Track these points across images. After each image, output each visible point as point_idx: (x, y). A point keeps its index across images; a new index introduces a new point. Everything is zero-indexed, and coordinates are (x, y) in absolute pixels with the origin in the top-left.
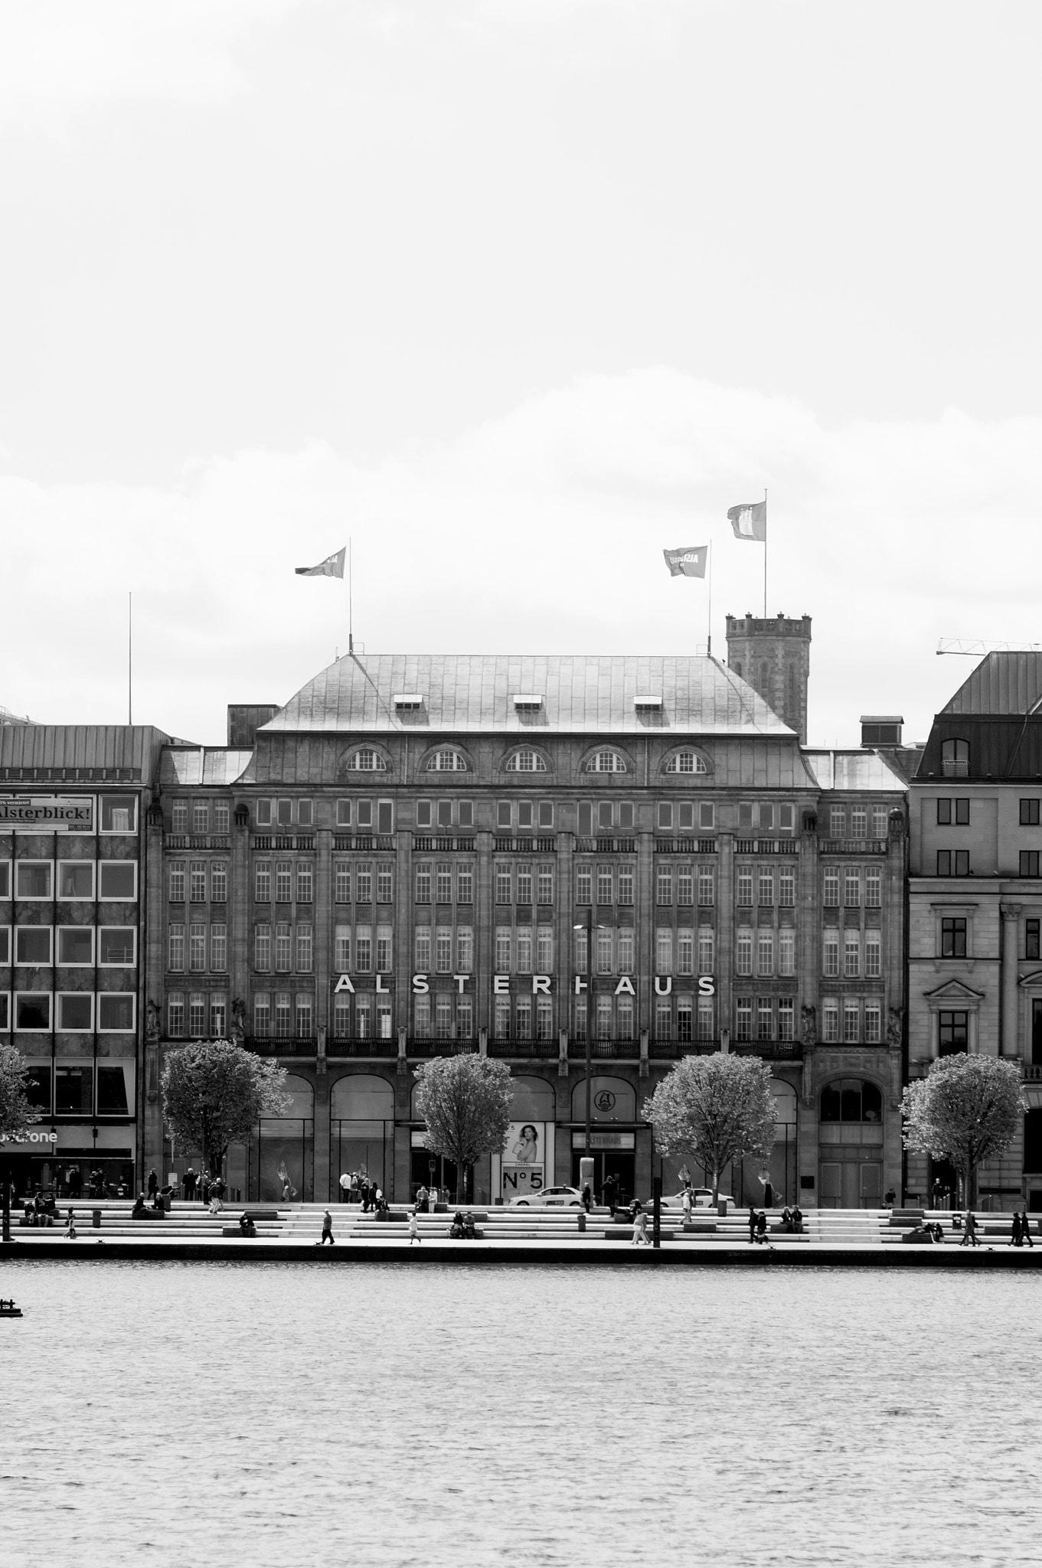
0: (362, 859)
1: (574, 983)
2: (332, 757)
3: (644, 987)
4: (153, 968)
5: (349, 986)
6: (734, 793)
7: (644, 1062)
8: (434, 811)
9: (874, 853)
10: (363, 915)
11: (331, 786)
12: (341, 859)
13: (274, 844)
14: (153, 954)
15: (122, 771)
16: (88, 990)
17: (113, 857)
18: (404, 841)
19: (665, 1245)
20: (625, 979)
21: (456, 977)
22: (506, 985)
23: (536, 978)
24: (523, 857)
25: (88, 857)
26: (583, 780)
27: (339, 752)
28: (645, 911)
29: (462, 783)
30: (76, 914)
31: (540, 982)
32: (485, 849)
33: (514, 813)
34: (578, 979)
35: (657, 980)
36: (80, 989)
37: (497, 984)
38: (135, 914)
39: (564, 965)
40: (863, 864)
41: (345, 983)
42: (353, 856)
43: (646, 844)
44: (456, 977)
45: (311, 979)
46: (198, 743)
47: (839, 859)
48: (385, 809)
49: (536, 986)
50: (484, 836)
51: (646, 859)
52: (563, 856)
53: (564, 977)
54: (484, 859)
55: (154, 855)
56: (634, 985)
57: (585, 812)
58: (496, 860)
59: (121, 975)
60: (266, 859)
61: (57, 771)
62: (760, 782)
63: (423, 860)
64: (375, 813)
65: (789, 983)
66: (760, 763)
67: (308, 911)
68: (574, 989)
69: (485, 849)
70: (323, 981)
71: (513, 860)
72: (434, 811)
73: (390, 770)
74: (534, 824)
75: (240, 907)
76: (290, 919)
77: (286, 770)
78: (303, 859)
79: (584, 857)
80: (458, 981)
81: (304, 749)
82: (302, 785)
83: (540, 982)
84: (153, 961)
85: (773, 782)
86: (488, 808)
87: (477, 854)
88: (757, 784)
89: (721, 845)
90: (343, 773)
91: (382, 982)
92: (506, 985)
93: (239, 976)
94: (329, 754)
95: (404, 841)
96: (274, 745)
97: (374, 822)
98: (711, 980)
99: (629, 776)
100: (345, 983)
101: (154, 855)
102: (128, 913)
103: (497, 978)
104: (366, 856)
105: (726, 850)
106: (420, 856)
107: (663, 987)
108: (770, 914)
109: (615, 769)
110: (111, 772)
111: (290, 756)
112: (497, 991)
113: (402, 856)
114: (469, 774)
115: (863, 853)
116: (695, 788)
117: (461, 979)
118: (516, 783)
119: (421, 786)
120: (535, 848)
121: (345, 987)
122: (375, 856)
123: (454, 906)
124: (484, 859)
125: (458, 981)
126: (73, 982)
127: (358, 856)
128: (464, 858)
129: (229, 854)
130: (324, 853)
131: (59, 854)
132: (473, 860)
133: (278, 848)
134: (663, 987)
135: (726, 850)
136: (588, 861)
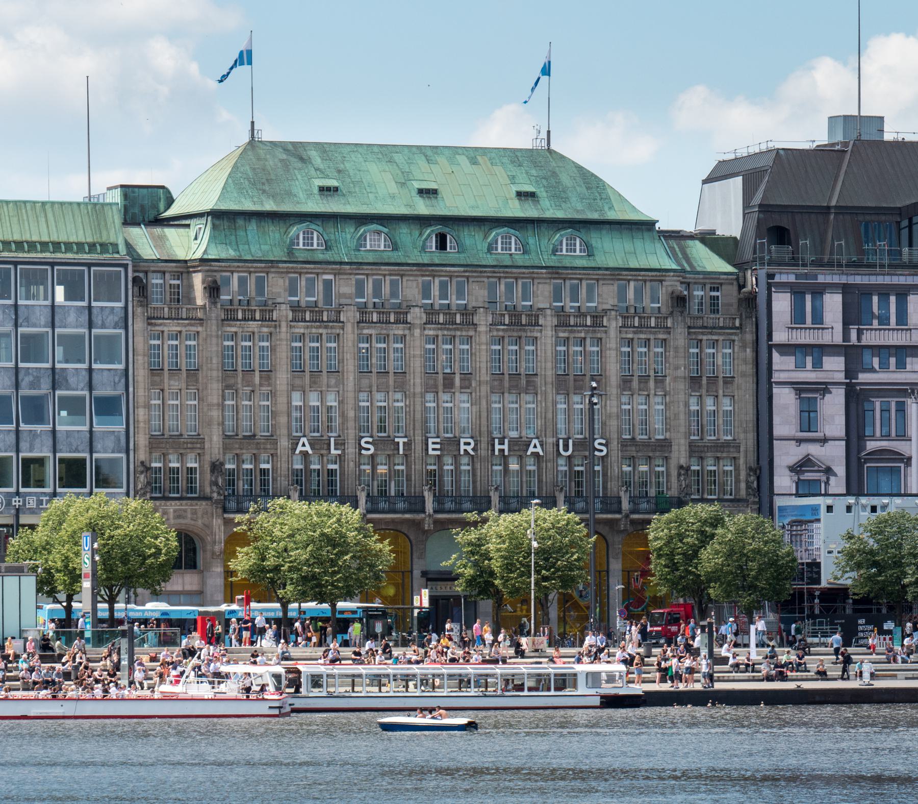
0: (314, 330)
1: (493, 445)
2: (277, 235)
3: (550, 448)
4: (141, 431)
5: (308, 448)
6: (617, 274)
7: (430, 515)
8: (369, 288)
9: (731, 328)
10: (315, 383)
11: (285, 262)
12: (297, 330)
13: (240, 316)
14: (141, 418)
15: (101, 245)
16: (83, 451)
17: (103, 326)
18: (350, 314)
19: (718, 686)
20: (535, 441)
21: (396, 440)
22: (438, 446)
23: (462, 441)
24: (448, 329)
25: (120, 452)
26: (490, 260)
27: (282, 231)
28: (549, 380)
29: (392, 261)
30: (72, 380)
31: (466, 444)
32: (418, 322)
33: (435, 290)
34: (497, 441)
35: (561, 442)
36: (77, 451)
37: (431, 446)
38: (123, 381)
39: (484, 429)
40: (721, 338)
41: (304, 445)
42: (308, 327)
43: (549, 318)
44: (396, 440)
45: (272, 439)
46: (647, 212)
47: (703, 333)
48: (328, 284)
49: (463, 447)
50: (417, 310)
51: (549, 332)
52: (482, 329)
53: (484, 439)
54: (417, 332)
55: (138, 325)
56: (542, 445)
57: (492, 289)
58: (426, 332)
59: (113, 437)
60: (234, 329)
61: (44, 245)
62: (633, 264)
63: (365, 331)
64: (320, 287)
65: (665, 446)
66: (628, 246)
67: (269, 378)
68: (493, 450)
69: (418, 322)
70: (284, 443)
71: (440, 333)
72: (369, 288)
73: (328, 248)
74: (455, 302)
75: (215, 374)
76: (254, 385)
77: (241, 247)
78: (265, 330)
79: (498, 330)
80: (398, 443)
81: (253, 226)
82: (261, 261)
83: (466, 444)
84: (142, 425)
85: (643, 264)
86: (415, 284)
87: (410, 326)
88: (632, 266)
89: (609, 320)
90: (290, 252)
91: (336, 444)
92: (438, 446)
93: (215, 438)
94: (274, 232)
95: (350, 314)
96: (226, 223)
97: (318, 296)
98: (604, 441)
99: (527, 257)
100: (304, 446)
101: (138, 325)
102: (117, 379)
103: (430, 441)
104: (317, 328)
105: (614, 324)
106: (363, 328)
107: (566, 448)
108: (647, 382)
109: (513, 251)
110: (92, 246)
111: (241, 233)
112: (431, 452)
113: (349, 327)
114: (395, 254)
115: (722, 328)
116: (584, 268)
117: (401, 441)
118: (437, 262)
119: (361, 264)
120: (458, 321)
121: (304, 449)
122: (326, 327)
123: (391, 374)
124: (417, 332)
125: (398, 443)
126: (71, 444)
127: (312, 327)
128: (399, 330)
129: (202, 325)
130: (284, 324)
131: (57, 323)
132: (407, 332)
133: (244, 319)
134: (566, 448)
135: (614, 324)
136: (501, 334)
